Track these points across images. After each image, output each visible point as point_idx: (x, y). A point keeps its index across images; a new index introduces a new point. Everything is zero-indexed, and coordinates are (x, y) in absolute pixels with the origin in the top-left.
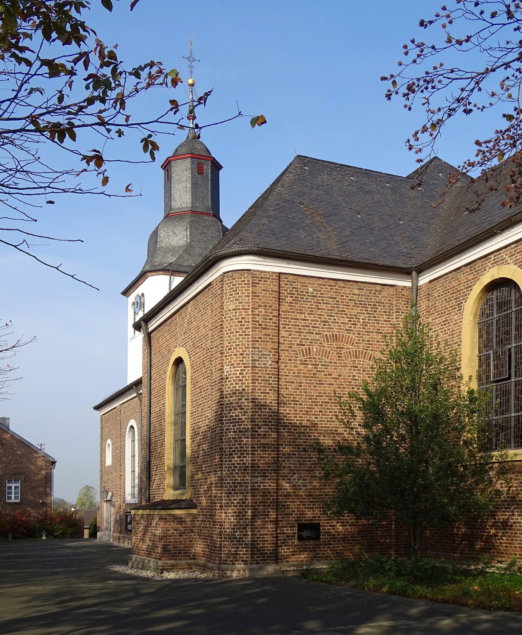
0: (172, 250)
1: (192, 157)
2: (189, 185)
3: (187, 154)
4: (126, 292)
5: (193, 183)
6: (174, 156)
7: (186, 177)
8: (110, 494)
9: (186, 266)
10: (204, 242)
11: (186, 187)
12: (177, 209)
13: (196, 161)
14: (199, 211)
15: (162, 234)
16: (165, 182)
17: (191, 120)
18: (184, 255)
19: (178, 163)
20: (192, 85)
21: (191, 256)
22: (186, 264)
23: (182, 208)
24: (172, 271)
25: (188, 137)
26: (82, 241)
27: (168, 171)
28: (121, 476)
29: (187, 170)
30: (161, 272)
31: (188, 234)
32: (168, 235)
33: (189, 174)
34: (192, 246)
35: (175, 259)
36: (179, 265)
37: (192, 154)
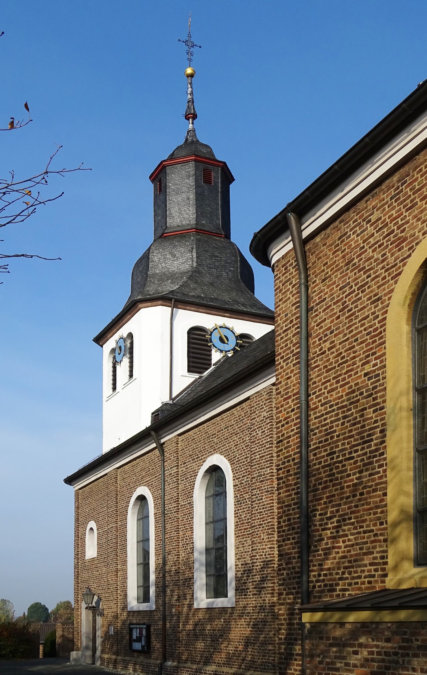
1: (195, 161)
2: (192, 196)
4: (101, 339)
6: (172, 157)
8: (96, 598)
9: (193, 296)
10: (216, 268)
11: (188, 199)
12: (175, 227)
13: (202, 166)
14: (207, 229)
15: (155, 257)
17: (191, 120)
19: (176, 168)
20: (191, 76)
22: (192, 294)
23: (182, 225)
25: (187, 140)
26: (63, 193)
28: (117, 571)
29: (189, 176)
30: (160, 302)
31: (195, 256)
33: (191, 181)
34: (199, 272)
35: (177, 287)
36: (184, 294)
37: (196, 156)
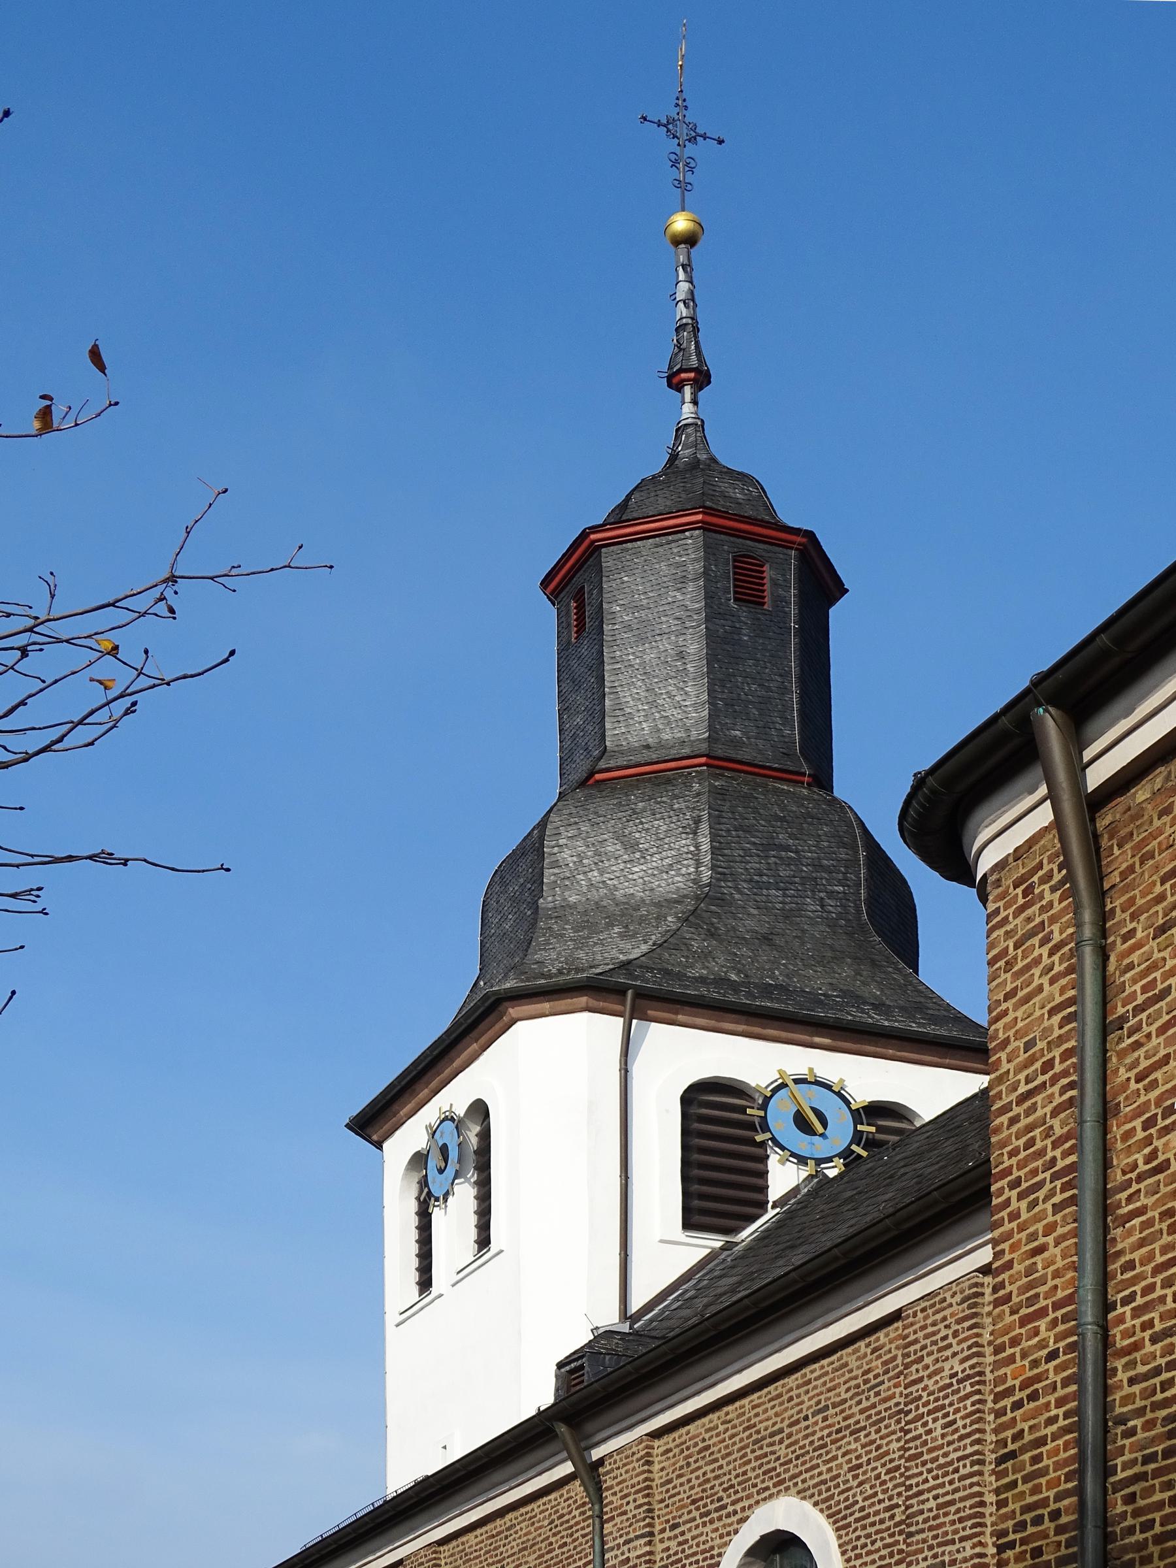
0: (627, 915)
1: (706, 527)
2: (695, 646)
3: (683, 511)
4: (374, 1122)
5: (712, 638)
6: (620, 515)
7: (681, 614)
9: (702, 980)
10: (782, 885)
11: (681, 656)
12: (632, 750)
13: (728, 546)
15: (566, 851)
16: (565, 650)
17: (688, 390)
18: (687, 932)
19: (638, 553)
20: (689, 240)
21: (721, 941)
22: (697, 971)
23: (661, 745)
24: (640, 994)
25: (674, 457)
27: (579, 597)
29: (684, 580)
30: (583, 1000)
31: (705, 846)
32: (597, 853)
33: (692, 597)
34: (721, 900)
35: (644, 948)
36: (667, 973)
37: (708, 511)
